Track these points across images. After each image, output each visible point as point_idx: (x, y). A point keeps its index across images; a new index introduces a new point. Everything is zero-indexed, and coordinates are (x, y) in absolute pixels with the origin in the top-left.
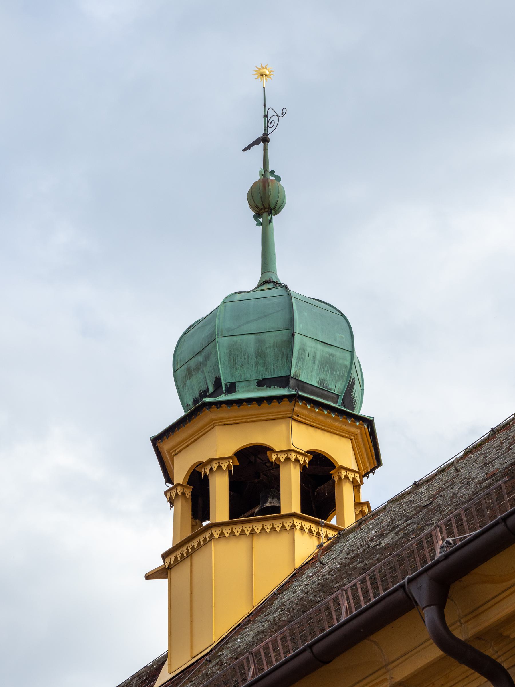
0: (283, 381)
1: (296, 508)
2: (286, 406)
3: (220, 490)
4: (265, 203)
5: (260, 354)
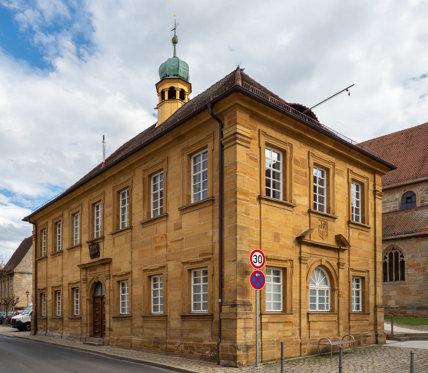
0: (177, 75)
1: (179, 98)
2: (178, 80)
3: (166, 94)
4: (175, 42)
5: (174, 70)
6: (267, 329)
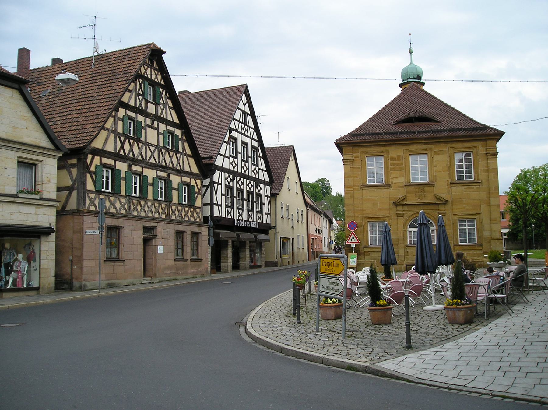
4: (411, 52)
6: (369, 255)
